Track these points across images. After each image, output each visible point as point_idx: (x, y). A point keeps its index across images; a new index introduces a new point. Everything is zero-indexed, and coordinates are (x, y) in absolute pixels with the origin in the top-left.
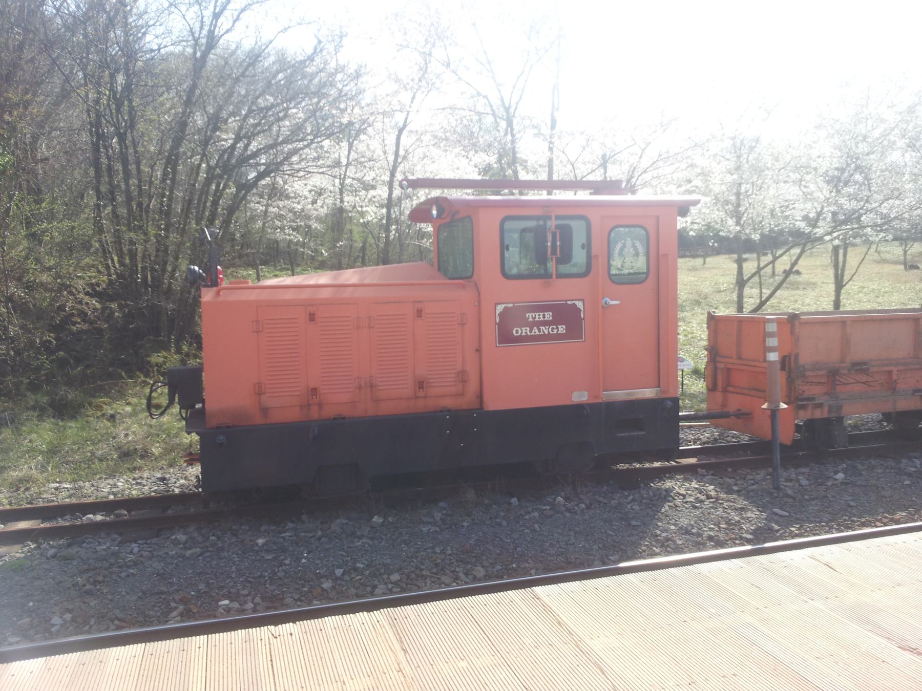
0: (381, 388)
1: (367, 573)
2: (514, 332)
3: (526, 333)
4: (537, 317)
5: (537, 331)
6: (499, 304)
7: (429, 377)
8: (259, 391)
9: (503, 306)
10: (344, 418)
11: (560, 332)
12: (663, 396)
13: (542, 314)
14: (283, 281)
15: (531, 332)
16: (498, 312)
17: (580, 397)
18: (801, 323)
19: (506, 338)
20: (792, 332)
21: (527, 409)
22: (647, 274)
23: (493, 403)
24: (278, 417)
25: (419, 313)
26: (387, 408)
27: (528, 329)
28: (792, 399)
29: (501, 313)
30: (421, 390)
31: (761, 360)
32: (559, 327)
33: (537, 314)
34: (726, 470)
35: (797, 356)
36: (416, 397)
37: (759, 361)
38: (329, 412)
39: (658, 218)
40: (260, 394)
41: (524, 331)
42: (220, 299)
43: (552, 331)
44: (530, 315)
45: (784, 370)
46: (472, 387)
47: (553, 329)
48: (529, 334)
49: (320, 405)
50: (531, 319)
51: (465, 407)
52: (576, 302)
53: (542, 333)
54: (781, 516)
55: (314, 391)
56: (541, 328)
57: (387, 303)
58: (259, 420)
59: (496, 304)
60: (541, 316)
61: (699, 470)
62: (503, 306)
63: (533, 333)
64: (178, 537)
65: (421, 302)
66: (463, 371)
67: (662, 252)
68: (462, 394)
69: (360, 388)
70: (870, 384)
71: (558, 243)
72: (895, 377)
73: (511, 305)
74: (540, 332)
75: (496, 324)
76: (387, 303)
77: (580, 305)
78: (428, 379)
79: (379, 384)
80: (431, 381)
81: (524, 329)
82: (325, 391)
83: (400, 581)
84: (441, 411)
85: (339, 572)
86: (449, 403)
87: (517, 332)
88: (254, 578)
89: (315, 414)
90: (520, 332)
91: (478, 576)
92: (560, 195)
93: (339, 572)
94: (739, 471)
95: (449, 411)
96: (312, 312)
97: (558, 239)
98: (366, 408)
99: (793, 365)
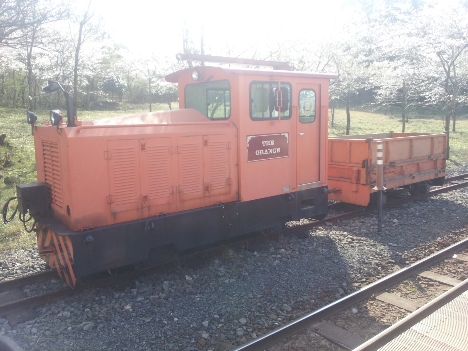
0: (185, 193)
1: (223, 320)
2: (256, 153)
3: (262, 153)
4: (267, 143)
5: (267, 152)
6: (249, 136)
7: (212, 183)
8: (110, 201)
9: (251, 137)
10: (165, 215)
11: (277, 152)
12: (322, 186)
13: (269, 141)
14: (109, 121)
15: (264, 152)
16: (248, 141)
17: (287, 190)
18: (373, 143)
19: (252, 157)
20: (369, 148)
21: (262, 199)
22: (315, 116)
23: (246, 197)
24: (122, 218)
25: (206, 143)
26: (188, 206)
27: (263, 151)
28: (368, 183)
29: (250, 141)
30: (207, 192)
31: (348, 162)
32: (277, 149)
33: (267, 142)
34: (337, 221)
35: (371, 160)
36: (205, 197)
37: (345, 163)
38: (155, 211)
39: (320, 85)
40: (110, 203)
41: (261, 152)
42: (80, 135)
43: (274, 152)
44: (264, 142)
45: (365, 168)
46: (234, 188)
47: (274, 150)
48: (263, 154)
49: (149, 207)
50: (264, 145)
51: (231, 200)
52: (285, 134)
53: (269, 153)
54: (394, 247)
55: (146, 197)
56: (269, 150)
57: (188, 136)
58: (110, 221)
59: (248, 136)
60: (269, 143)
61: (326, 223)
62: (251, 137)
63: (265, 153)
64: (63, 314)
65: (207, 135)
66: (229, 179)
67: (322, 105)
68: (229, 193)
69: (173, 194)
70: (395, 172)
71: (282, 99)
72: (404, 168)
73: (255, 137)
74: (268, 152)
75: (247, 148)
76: (188, 136)
77: (286, 135)
78: (211, 184)
79: (184, 190)
80: (213, 186)
81: (261, 151)
82: (153, 198)
83: (247, 323)
84: (219, 205)
85: (206, 323)
86: (222, 199)
87: (257, 153)
88: (153, 340)
89: (146, 214)
90: (259, 153)
91: (288, 310)
92: (225, 66)
93: (206, 323)
94: (343, 221)
95: (223, 204)
96: (143, 144)
97: (282, 97)
98: (177, 207)
99: (369, 164)
